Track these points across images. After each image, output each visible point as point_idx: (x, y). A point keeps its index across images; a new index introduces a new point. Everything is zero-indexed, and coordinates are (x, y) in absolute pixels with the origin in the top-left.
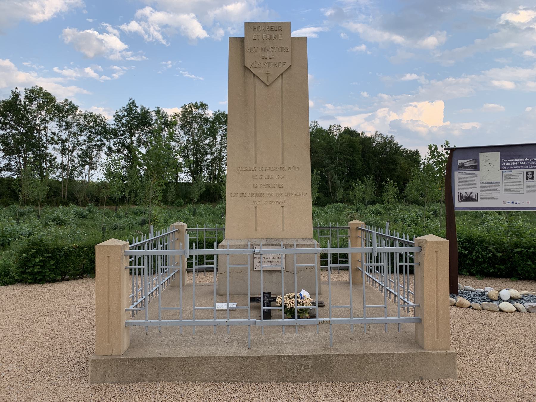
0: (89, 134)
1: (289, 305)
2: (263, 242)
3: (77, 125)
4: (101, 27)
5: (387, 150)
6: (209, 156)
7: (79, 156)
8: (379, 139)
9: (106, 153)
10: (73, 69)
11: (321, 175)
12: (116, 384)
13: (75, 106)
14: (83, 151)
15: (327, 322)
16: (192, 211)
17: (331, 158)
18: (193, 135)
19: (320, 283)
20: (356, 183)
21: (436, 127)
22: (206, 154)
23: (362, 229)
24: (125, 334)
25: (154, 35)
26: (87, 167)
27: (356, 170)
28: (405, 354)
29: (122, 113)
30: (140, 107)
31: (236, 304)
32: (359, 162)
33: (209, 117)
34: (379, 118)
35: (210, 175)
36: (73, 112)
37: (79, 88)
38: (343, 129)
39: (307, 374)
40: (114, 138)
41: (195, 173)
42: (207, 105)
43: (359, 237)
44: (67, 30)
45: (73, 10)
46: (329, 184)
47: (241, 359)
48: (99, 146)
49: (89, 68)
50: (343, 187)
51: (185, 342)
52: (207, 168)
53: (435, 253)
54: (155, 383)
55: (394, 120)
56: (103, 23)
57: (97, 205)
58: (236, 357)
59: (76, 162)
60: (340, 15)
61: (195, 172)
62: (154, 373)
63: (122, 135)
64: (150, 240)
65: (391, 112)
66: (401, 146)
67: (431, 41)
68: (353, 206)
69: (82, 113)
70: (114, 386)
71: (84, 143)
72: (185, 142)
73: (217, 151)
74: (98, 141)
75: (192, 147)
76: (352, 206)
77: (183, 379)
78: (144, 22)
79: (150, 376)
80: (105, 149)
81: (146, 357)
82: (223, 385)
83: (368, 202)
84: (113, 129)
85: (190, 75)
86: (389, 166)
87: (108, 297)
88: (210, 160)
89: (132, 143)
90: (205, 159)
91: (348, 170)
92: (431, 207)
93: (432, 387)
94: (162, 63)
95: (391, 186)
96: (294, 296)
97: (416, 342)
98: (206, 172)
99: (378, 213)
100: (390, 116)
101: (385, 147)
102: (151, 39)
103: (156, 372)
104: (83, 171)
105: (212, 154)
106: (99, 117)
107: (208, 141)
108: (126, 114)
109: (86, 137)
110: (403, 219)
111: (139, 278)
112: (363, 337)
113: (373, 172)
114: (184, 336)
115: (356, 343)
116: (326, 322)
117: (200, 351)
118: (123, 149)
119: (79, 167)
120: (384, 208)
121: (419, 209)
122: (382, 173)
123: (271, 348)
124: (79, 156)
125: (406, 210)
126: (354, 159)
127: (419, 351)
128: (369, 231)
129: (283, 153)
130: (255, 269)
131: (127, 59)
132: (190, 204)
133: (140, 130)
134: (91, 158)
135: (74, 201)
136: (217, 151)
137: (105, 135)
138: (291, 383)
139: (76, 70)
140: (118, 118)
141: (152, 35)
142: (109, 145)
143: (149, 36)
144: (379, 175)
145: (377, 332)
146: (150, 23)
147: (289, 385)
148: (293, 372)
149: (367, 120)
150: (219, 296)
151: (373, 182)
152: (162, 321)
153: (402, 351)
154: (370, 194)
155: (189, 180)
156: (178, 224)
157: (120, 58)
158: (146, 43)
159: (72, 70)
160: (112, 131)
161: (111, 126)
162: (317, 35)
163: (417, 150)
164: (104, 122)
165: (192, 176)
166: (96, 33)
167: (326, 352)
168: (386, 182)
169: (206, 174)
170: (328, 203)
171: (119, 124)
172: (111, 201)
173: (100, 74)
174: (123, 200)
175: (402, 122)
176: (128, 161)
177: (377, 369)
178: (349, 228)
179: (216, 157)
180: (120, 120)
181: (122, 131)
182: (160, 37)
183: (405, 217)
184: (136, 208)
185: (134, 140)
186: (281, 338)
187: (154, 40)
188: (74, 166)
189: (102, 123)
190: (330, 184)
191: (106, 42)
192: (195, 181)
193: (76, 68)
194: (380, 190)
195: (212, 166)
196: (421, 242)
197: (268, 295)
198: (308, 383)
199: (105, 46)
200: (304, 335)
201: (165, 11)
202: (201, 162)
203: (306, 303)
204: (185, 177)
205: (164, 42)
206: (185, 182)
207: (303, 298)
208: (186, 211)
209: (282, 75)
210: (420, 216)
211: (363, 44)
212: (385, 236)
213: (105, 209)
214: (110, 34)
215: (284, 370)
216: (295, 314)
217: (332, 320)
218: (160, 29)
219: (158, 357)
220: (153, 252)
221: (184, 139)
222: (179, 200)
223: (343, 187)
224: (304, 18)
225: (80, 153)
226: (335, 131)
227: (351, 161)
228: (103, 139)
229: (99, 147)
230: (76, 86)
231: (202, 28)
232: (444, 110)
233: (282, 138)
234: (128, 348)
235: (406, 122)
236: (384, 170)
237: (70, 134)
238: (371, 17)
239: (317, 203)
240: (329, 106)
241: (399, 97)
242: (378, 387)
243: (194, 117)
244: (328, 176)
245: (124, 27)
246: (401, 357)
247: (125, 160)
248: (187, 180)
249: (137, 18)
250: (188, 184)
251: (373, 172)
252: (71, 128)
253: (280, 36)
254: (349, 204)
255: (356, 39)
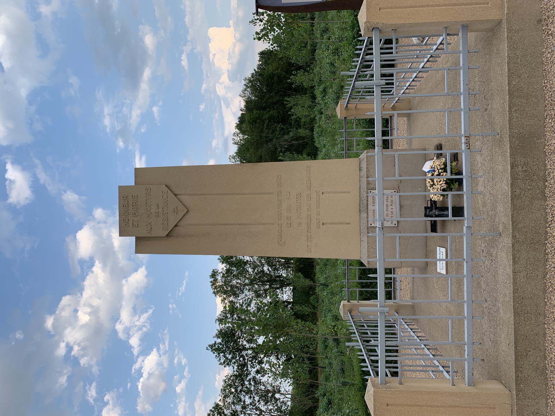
0: (243, 393)
1: (443, 185)
2: (364, 215)
3: (234, 405)
4: (136, 374)
5: (259, 84)
6: (265, 268)
7: (266, 404)
8: (248, 93)
9: (263, 376)
10: (177, 405)
11: (284, 152)
12: (550, 401)
13: (214, 406)
14: (261, 399)
15: (467, 140)
16: (323, 288)
17: (267, 142)
18: (244, 285)
19: (410, 150)
20: (293, 115)
21: (235, 34)
22: (263, 271)
23: (347, 103)
24: (483, 386)
25: (144, 321)
26: (277, 396)
27: (280, 115)
28: (508, 42)
29: (221, 359)
30: (216, 339)
31: (438, 248)
32: (271, 113)
33: (225, 268)
34: (226, 93)
35: (285, 268)
36: (221, 408)
37: (197, 399)
38: (237, 130)
39: (535, 163)
40: (247, 367)
41: (283, 283)
42: (213, 270)
43: (356, 107)
44: (139, 408)
45: (119, 402)
46: (293, 144)
47: (515, 245)
48: (255, 383)
49: (177, 389)
50: (297, 129)
51: (492, 312)
52: (278, 270)
53: (382, 10)
54: (547, 352)
55: (229, 77)
56: (132, 372)
57: (317, 387)
58: (512, 252)
59: (272, 408)
60: (124, 132)
61: (281, 283)
62: (534, 354)
63: (244, 359)
64: (364, 348)
65: (220, 81)
66: (255, 70)
67: (149, 41)
68: (317, 118)
69: (222, 400)
70: (552, 403)
71: (252, 398)
72: (251, 293)
73: (260, 260)
74: (250, 384)
75: (256, 286)
76: (317, 119)
77: (543, 317)
78: (130, 332)
79: (538, 359)
80: (258, 376)
81: (513, 362)
82: (550, 268)
83: (312, 102)
84: (238, 368)
85: (183, 284)
86: (275, 82)
87: (437, 406)
88: (270, 268)
89: (252, 348)
90: (268, 272)
91: (279, 124)
92: (319, 36)
93: (553, 6)
94: (171, 314)
95: (297, 78)
96: (430, 179)
97: (492, 30)
98: (282, 272)
99: (325, 91)
100: (224, 82)
101: (256, 86)
102: (147, 324)
103: (533, 351)
104: (281, 400)
105: (263, 265)
106: (226, 382)
107: (250, 269)
108: (223, 354)
109: (246, 396)
110: (332, 64)
111: (402, 351)
112: (483, 96)
113: (281, 98)
114: (483, 312)
115: (492, 104)
116: (467, 141)
117: (505, 295)
118: (258, 358)
119: (277, 404)
120: (319, 86)
121: (320, 49)
122: (282, 89)
123: (500, 208)
124: (266, 404)
125: (321, 63)
126: (268, 118)
127: (505, 25)
128: (350, 94)
129: (262, 194)
130: (396, 225)
131: (167, 349)
132: (315, 289)
133: (239, 340)
134: (268, 391)
135: (312, 411)
136: (260, 260)
137: (244, 376)
138: (546, 184)
139: (179, 401)
140: (227, 363)
141: (144, 324)
142: (255, 373)
143: (144, 326)
144: (285, 92)
145: (477, 79)
146: (132, 325)
147: (550, 186)
148: (533, 180)
149: (228, 105)
150: (428, 267)
151: (292, 98)
152: (466, 340)
153: (504, 47)
154: (305, 100)
155: (291, 289)
156: (342, 311)
157: (167, 356)
158: (151, 330)
159: (178, 406)
160: (240, 369)
161: (235, 370)
162: (143, 156)
163: (259, 54)
164: (231, 376)
165: (286, 287)
166: (141, 380)
167: (507, 140)
168: (292, 84)
169: (284, 271)
170: (313, 144)
171: (233, 361)
172: (313, 373)
173: (182, 377)
174: (313, 360)
175: (230, 68)
176: (271, 353)
177: (528, 77)
178: (345, 118)
179: (266, 261)
180: (228, 361)
181: (240, 358)
182: (145, 315)
183: (330, 62)
184: (320, 346)
185: (250, 346)
186: (484, 196)
187: (149, 321)
188: (277, 410)
189: (232, 378)
190: (293, 142)
191: (151, 370)
192: (291, 283)
193: (177, 401)
194: (300, 90)
195: (275, 265)
196: (367, 29)
197: (428, 210)
198: (547, 162)
199: (155, 371)
200: (480, 167)
201: (120, 309)
202: (271, 276)
203: (439, 165)
204: (287, 294)
205: (150, 311)
206: (292, 293)
207: (433, 169)
208: (323, 294)
209: (175, 195)
210: (328, 47)
211: (152, 109)
212: (356, 76)
213: (321, 378)
214: (143, 366)
215: (530, 192)
216: (453, 179)
217: (465, 133)
218: (138, 315)
219: (514, 348)
220: (380, 351)
221: (248, 294)
222: (311, 300)
223: (297, 129)
224: (126, 169)
225: (262, 403)
226: (239, 138)
227: (270, 121)
228: (248, 379)
229: (257, 382)
230: (194, 402)
231: (136, 273)
232: (217, 27)
233: (245, 194)
234: (501, 383)
235: (230, 65)
236: (280, 87)
237: (243, 413)
238: (125, 101)
239: (313, 154)
240: (214, 143)
241: (205, 73)
242: (553, 74)
243: (226, 283)
244: (285, 145)
245: (136, 351)
246: (512, 47)
247: (270, 356)
248: (290, 292)
249: (126, 338)
250: (294, 291)
251: (281, 98)
252: (237, 411)
253: (134, 198)
254: (315, 122)
255: (146, 117)
